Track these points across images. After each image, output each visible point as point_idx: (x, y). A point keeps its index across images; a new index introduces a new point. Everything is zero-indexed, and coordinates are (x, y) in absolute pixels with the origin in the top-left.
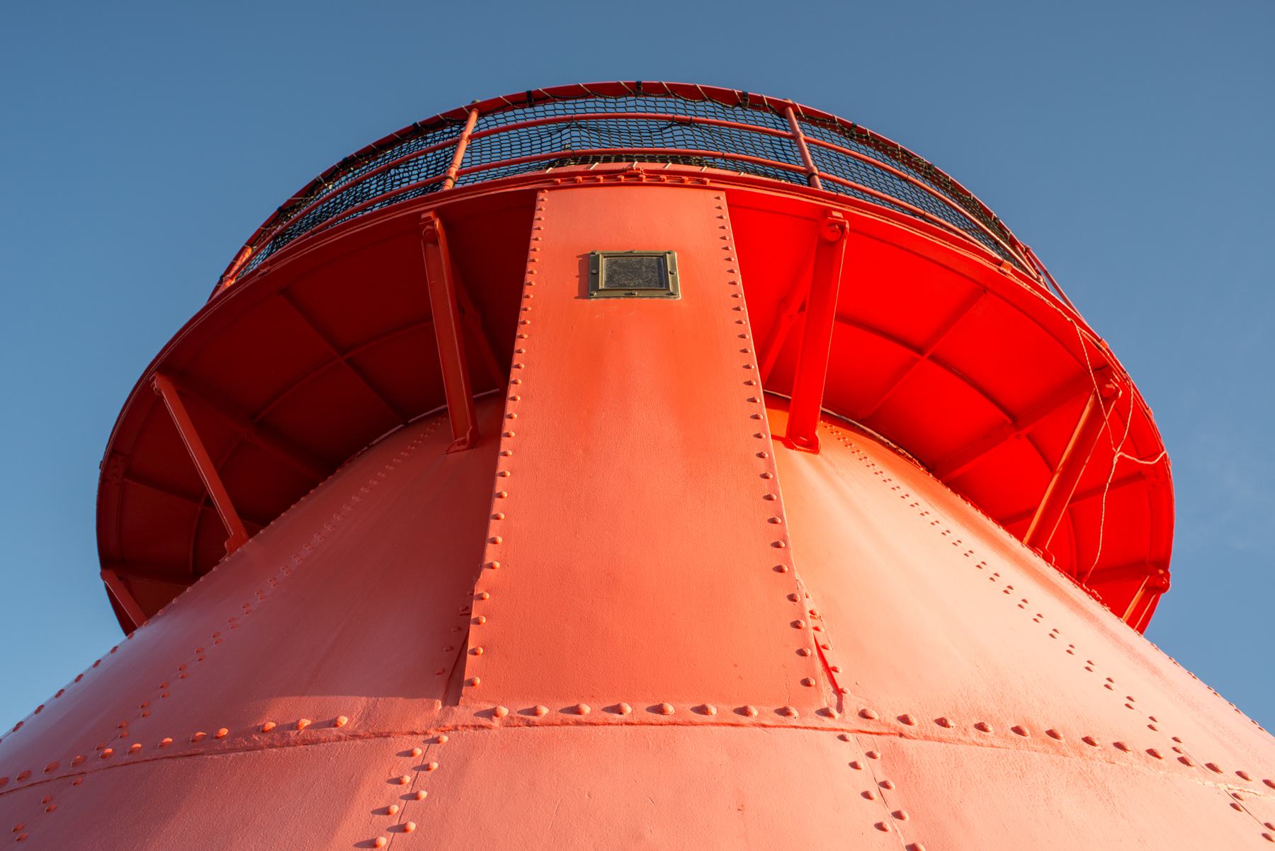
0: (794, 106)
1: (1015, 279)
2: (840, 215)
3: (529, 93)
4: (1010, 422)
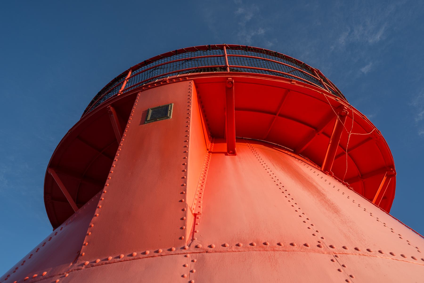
0: (226, 46)
1: (297, 85)
2: (231, 79)
3: (145, 61)
4: (315, 130)
